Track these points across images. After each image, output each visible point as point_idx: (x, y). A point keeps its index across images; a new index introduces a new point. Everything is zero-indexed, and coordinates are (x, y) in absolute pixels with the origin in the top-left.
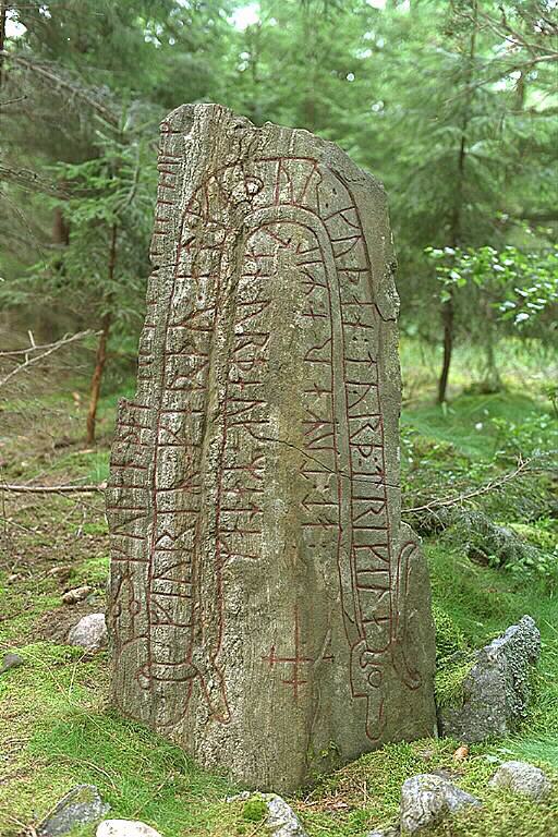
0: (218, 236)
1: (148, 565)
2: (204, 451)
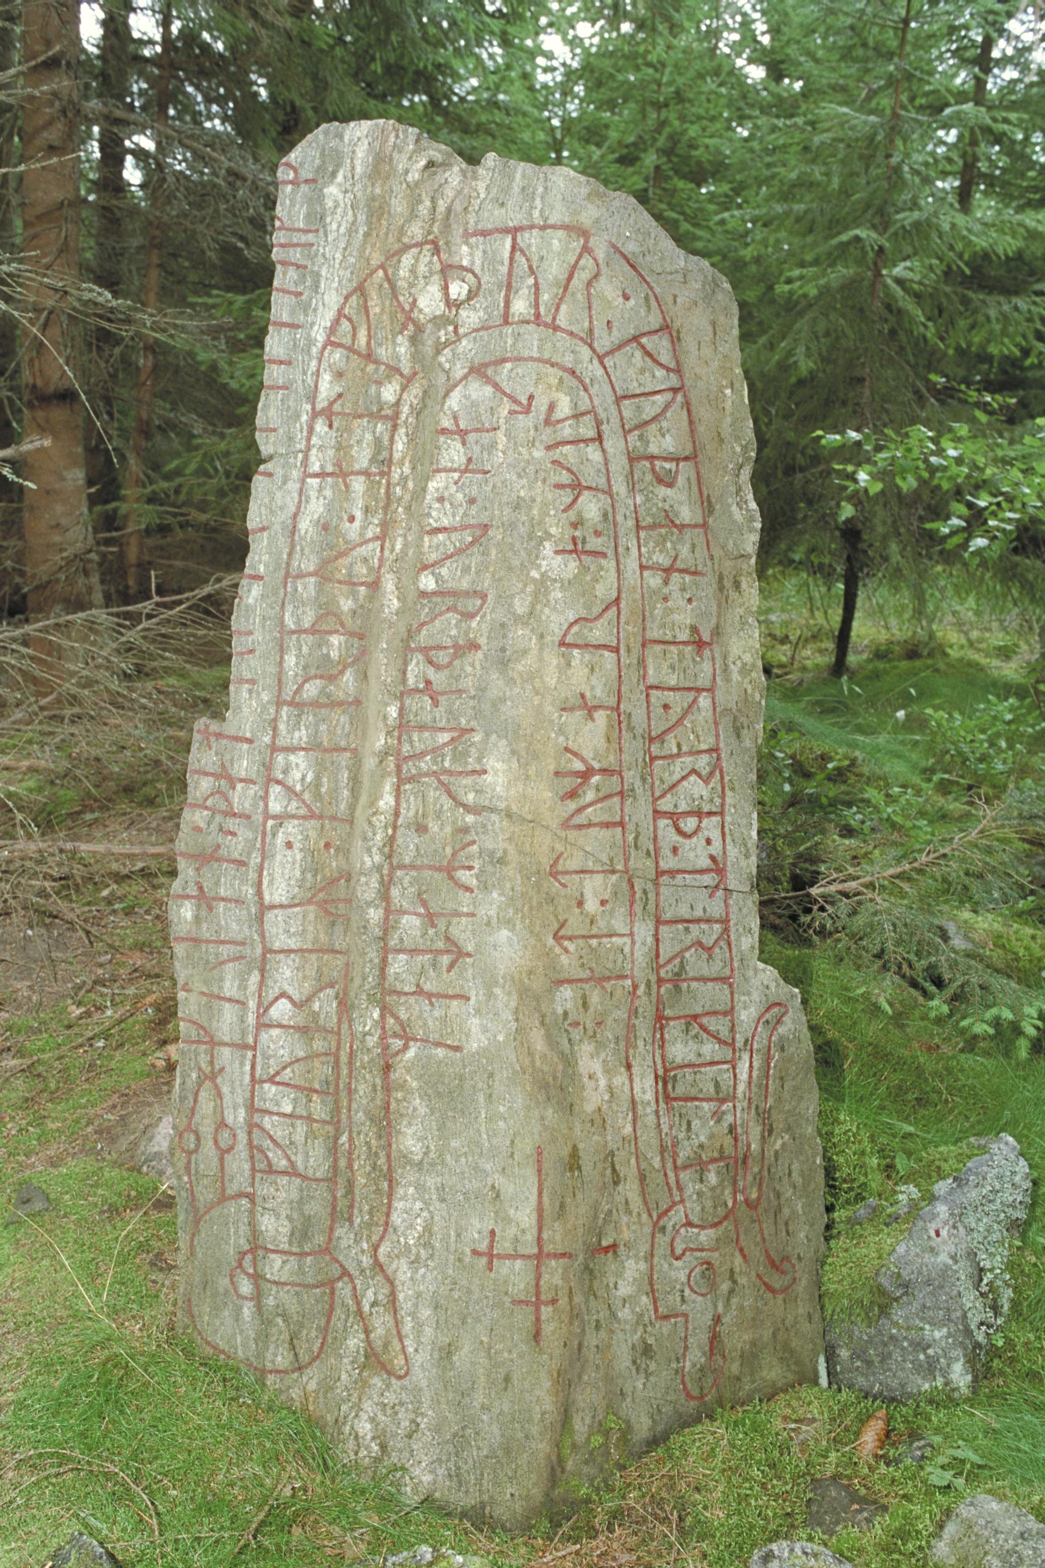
0: (389, 393)
1: (250, 1054)
2: (358, 832)
